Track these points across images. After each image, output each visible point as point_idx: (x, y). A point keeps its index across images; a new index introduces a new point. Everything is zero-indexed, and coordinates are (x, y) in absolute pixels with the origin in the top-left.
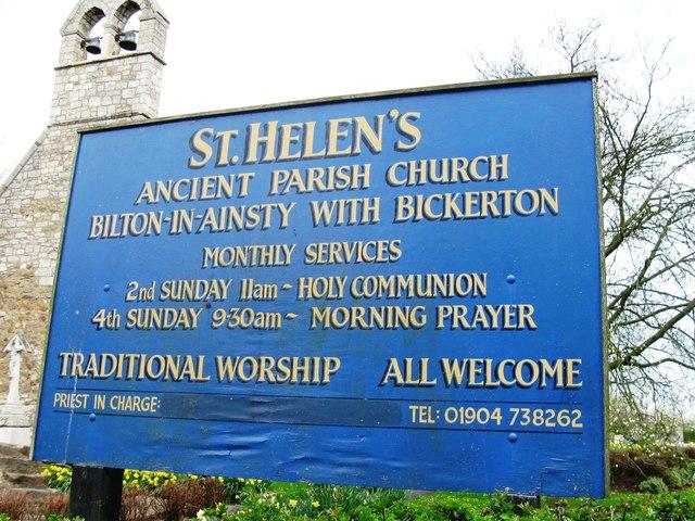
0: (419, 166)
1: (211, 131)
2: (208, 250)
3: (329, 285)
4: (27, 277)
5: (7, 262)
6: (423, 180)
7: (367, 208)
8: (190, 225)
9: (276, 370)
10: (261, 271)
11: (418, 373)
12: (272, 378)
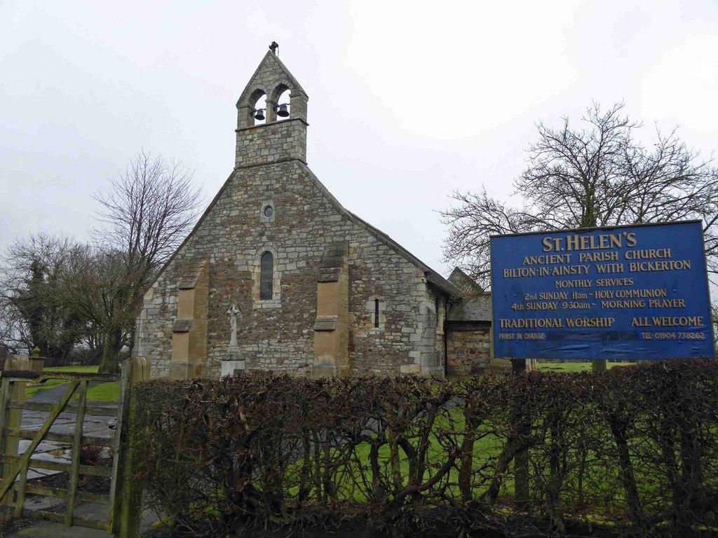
0: (637, 252)
1: (550, 238)
2: (557, 282)
3: (606, 293)
4: (229, 266)
5: (215, 257)
6: (639, 258)
7: (618, 267)
8: (547, 273)
9: (590, 323)
10: (580, 290)
11: (644, 322)
12: (589, 325)
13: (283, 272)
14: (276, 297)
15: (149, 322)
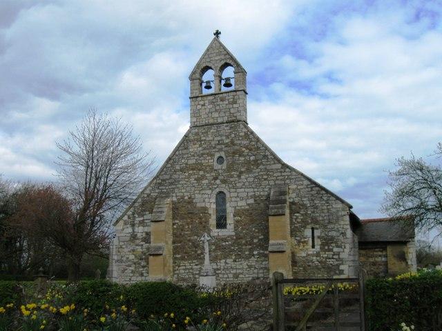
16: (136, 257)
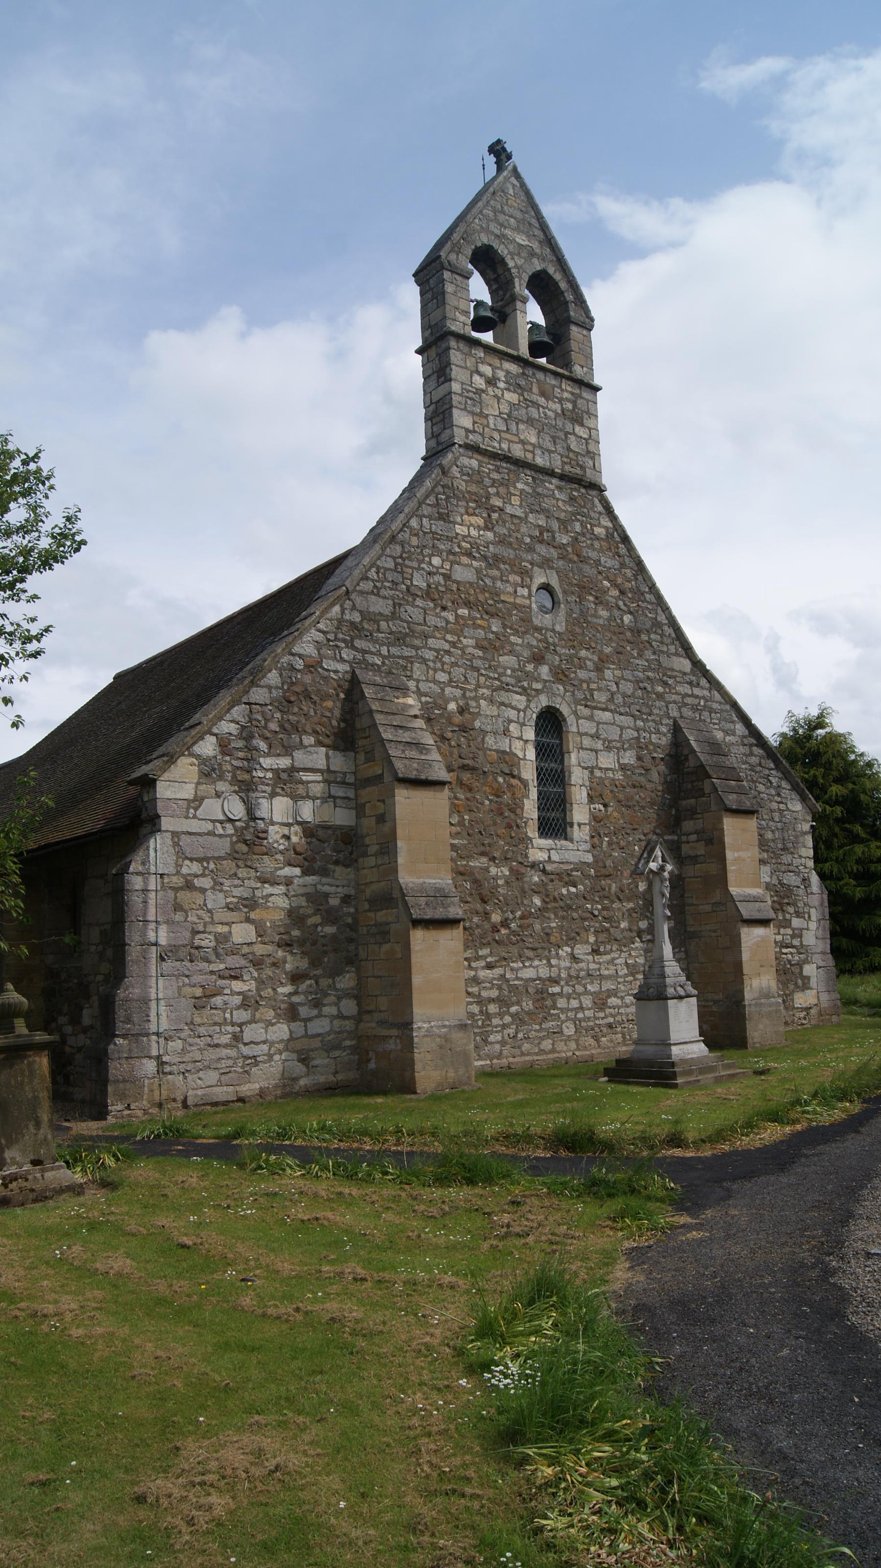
13: (591, 770)
14: (580, 834)
15: (189, 886)
16: (261, 933)
